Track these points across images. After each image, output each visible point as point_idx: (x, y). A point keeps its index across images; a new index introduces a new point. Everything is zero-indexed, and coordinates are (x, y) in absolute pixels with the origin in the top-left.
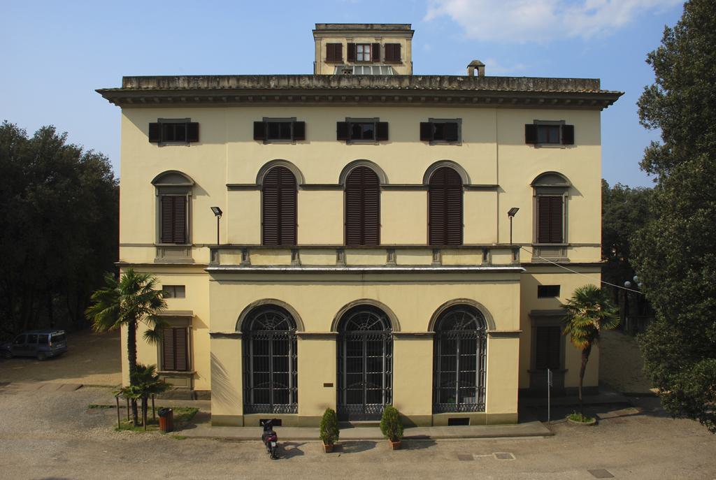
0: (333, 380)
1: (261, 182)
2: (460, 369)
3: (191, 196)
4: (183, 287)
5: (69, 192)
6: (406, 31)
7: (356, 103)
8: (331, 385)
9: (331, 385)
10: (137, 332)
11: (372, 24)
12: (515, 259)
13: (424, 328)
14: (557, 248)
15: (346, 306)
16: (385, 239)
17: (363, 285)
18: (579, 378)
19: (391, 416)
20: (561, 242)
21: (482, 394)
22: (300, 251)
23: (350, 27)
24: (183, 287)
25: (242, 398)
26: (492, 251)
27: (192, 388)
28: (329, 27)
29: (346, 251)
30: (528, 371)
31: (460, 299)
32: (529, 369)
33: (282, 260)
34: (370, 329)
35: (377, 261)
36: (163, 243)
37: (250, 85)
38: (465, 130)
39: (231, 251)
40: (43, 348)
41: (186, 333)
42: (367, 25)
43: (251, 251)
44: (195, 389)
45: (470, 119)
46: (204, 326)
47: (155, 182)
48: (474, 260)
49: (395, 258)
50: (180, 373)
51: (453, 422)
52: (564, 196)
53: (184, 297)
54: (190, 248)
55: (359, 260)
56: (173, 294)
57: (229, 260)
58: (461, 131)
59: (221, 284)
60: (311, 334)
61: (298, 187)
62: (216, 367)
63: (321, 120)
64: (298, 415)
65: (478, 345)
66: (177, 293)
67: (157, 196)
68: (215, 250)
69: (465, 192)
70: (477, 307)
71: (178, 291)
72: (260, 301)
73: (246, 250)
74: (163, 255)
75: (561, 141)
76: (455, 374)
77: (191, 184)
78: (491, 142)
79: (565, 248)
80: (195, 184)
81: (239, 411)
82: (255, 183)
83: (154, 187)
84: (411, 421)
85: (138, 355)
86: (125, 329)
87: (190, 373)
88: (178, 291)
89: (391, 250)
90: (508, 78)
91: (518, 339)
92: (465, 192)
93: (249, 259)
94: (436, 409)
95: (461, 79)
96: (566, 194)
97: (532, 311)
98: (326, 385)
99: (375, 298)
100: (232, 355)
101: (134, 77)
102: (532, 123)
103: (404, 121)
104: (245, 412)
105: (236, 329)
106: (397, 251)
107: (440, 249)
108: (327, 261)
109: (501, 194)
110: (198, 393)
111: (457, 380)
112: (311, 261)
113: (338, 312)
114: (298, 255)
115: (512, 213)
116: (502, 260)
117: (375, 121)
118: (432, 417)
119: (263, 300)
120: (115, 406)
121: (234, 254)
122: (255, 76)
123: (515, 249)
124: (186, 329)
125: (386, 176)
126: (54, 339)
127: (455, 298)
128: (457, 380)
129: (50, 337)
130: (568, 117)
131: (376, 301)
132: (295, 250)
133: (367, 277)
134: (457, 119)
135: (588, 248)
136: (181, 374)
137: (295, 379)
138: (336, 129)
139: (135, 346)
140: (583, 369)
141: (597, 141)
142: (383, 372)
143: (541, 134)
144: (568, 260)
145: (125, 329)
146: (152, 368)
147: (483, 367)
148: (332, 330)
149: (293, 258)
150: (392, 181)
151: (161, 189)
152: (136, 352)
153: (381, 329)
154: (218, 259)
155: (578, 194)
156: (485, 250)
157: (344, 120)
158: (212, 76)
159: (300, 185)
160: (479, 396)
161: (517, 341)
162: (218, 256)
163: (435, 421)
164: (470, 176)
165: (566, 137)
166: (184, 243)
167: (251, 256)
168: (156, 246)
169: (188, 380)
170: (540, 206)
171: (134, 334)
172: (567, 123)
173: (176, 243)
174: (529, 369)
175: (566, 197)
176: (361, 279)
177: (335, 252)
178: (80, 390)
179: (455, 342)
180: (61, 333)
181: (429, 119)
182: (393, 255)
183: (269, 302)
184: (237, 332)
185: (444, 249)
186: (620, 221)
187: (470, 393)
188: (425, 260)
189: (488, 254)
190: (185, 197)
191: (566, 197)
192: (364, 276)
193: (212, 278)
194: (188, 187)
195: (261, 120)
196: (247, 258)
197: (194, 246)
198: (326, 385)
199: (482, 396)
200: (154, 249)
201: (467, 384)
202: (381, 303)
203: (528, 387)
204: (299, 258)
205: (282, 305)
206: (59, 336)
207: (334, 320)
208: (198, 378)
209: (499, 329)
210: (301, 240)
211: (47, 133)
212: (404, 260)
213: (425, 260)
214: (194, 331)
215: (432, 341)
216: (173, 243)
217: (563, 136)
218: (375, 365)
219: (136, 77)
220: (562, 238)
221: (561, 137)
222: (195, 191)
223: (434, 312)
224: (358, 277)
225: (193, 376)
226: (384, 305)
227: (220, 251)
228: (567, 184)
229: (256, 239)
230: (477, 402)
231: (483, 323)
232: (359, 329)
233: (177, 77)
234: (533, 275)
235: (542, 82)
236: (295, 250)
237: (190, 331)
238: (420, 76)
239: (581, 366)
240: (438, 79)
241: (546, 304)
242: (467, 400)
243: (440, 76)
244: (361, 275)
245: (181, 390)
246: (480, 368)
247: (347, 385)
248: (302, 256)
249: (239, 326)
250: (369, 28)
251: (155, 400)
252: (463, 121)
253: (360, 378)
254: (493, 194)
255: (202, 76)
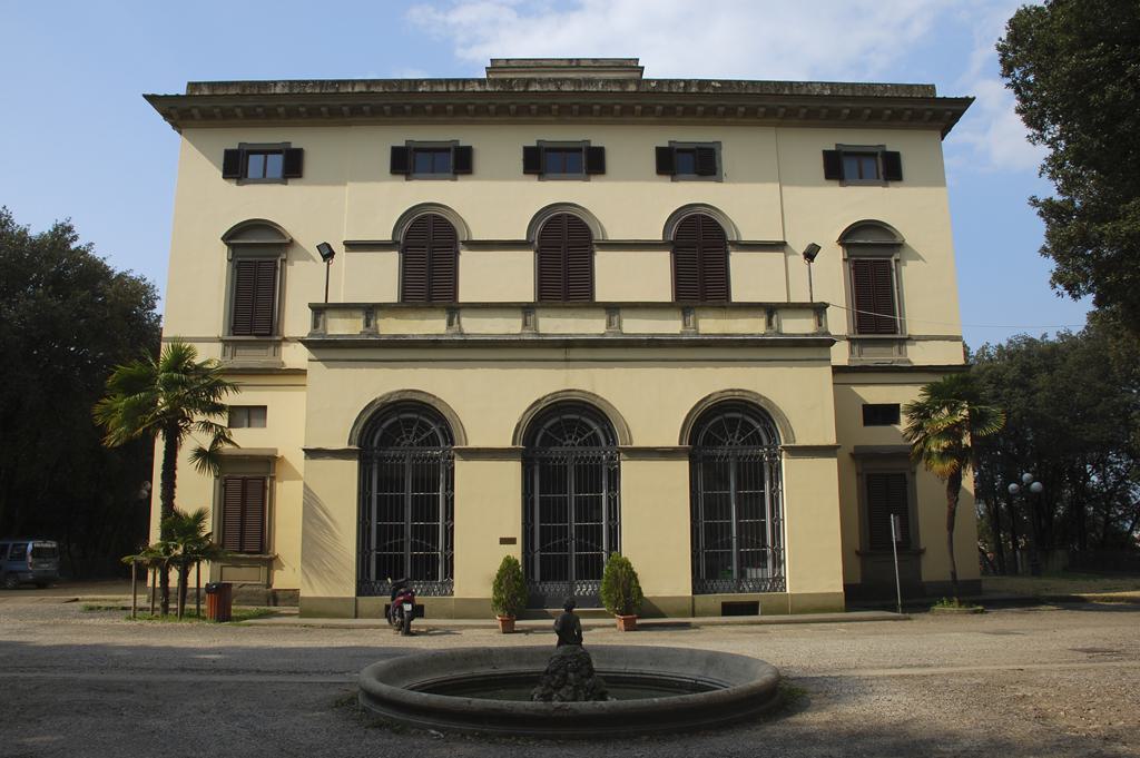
0: (516, 531)
1: (401, 238)
2: (738, 518)
3: (285, 260)
4: (264, 408)
5: (87, 309)
6: (638, 60)
7: (553, 119)
8: (512, 541)
9: (512, 541)
10: (179, 453)
11: (578, 60)
12: (820, 325)
13: (673, 440)
14: (890, 342)
15: (538, 402)
16: (602, 294)
17: (567, 368)
18: (946, 533)
19: (621, 568)
20: (895, 333)
21: (778, 562)
22: (462, 313)
23: (544, 63)
24: (264, 408)
25: (354, 570)
26: (781, 313)
27: (269, 585)
28: (513, 64)
29: (538, 312)
30: (857, 553)
31: (732, 390)
32: (858, 549)
33: (432, 325)
34: (580, 444)
35: (592, 326)
36: (234, 335)
37: (380, 90)
38: (728, 158)
39: (347, 313)
40: (18, 566)
41: (264, 487)
42: (571, 60)
43: (380, 313)
44: (274, 587)
45: (734, 145)
46: (295, 476)
47: (227, 238)
48: (754, 326)
49: (620, 322)
50: (248, 556)
51: (729, 609)
52: (893, 260)
53: (265, 426)
54: (278, 344)
55: (555, 325)
56: (246, 421)
57: (340, 327)
58: (720, 161)
59: (329, 367)
60: (478, 449)
61: (461, 245)
62: (312, 508)
63: (499, 146)
64: (456, 596)
65: (767, 474)
66: (253, 420)
67: (229, 260)
68: (319, 310)
69: (733, 253)
70: (761, 403)
71: (255, 414)
72: (391, 394)
73: (370, 310)
74: (234, 355)
75: (881, 176)
76: (729, 525)
77: (287, 241)
78: (773, 181)
79: (904, 341)
80: (292, 241)
81: (350, 591)
82: (390, 239)
83: (226, 247)
84: (655, 607)
85: (178, 492)
86: (160, 445)
87: (268, 557)
88: (255, 414)
89: (613, 309)
90: (791, 83)
91: (835, 460)
92: (733, 253)
93: (376, 325)
94: (698, 587)
95: (718, 85)
96: (897, 256)
97: (855, 447)
98: (504, 541)
99: (588, 390)
100: (341, 486)
101: (205, 83)
102: (834, 149)
103: (631, 147)
104: (359, 592)
105: (350, 443)
106: (622, 312)
107: (692, 308)
108: (510, 326)
109: (790, 258)
110: (279, 594)
111: (734, 535)
112: (474, 326)
113: (525, 413)
114: (458, 318)
115: (811, 254)
116: (799, 326)
117: (583, 146)
118: (693, 599)
119: (397, 392)
120: (130, 608)
121: (351, 317)
122: (395, 80)
123: (819, 309)
124: (264, 480)
125: (602, 228)
126: (37, 552)
127: (722, 389)
128: (734, 535)
129: (30, 547)
130: (891, 141)
131: (589, 393)
132: (454, 309)
133: (574, 353)
134: (713, 143)
135: (940, 342)
136: (250, 559)
137: (450, 532)
138: (522, 157)
139: (175, 476)
140: (952, 514)
141: (939, 180)
142: (604, 494)
143: (849, 166)
144: (909, 362)
145: (160, 445)
146: (200, 516)
147: (778, 510)
148: (514, 443)
149: (450, 324)
150: (612, 236)
151: (239, 251)
152: (175, 487)
153: (598, 443)
154: (324, 325)
155: (918, 257)
156: (770, 310)
157: (535, 144)
158: (328, 81)
159: (463, 242)
160: (774, 567)
161: (831, 465)
162: (324, 320)
163: (698, 607)
164: (737, 225)
165: (891, 170)
166: (270, 335)
167: (380, 321)
168: (222, 341)
169: (264, 570)
170: (856, 274)
171: (175, 456)
172: (889, 149)
173: (256, 335)
174: (858, 549)
175: (897, 261)
176: (563, 357)
177: (519, 313)
178: (74, 604)
179: (726, 466)
180: (51, 545)
181: (670, 142)
182: (616, 318)
183: (407, 396)
184: (351, 447)
185: (702, 307)
186: (991, 386)
187: (758, 560)
188: (671, 326)
189: (775, 316)
190: (276, 262)
191: (897, 261)
192: (567, 349)
193: (313, 357)
194: (280, 245)
195: (403, 144)
196: (372, 323)
197: (285, 340)
198: (504, 541)
199: (780, 567)
200: (219, 346)
201: (758, 543)
202: (598, 396)
203: (859, 581)
204: (459, 323)
205: (430, 400)
206: (47, 548)
207: (518, 425)
208: (281, 567)
209: (801, 441)
210: (464, 296)
211: (62, 234)
212: (634, 326)
213: (671, 326)
214: (278, 484)
215: (688, 462)
216: (250, 335)
217: (884, 168)
218: (589, 509)
219: (208, 83)
220: (896, 327)
221: (881, 170)
222: (292, 253)
223: (688, 412)
224: (559, 354)
225: (271, 563)
226: (602, 399)
227: (328, 313)
228: (898, 240)
229: (392, 296)
230: (770, 575)
231: (772, 433)
232: (561, 445)
233: (272, 82)
234: (853, 388)
235: (844, 88)
236: (454, 309)
237: (271, 485)
238: (653, 80)
239: (946, 509)
240: (682, 84)
241: (880, 436)
242: (753, 573)
243: (684, 81)
244: (564, 350)
245: (249, 588)
246: (772, 516)
247: (542, 544)
248: (464, 320)
249: (355, 438)
250: (574, 64)
251: (195, 586)
252: (723, 145)
253: (563, 504)
254: (778, 256)
255: (313, 81)
